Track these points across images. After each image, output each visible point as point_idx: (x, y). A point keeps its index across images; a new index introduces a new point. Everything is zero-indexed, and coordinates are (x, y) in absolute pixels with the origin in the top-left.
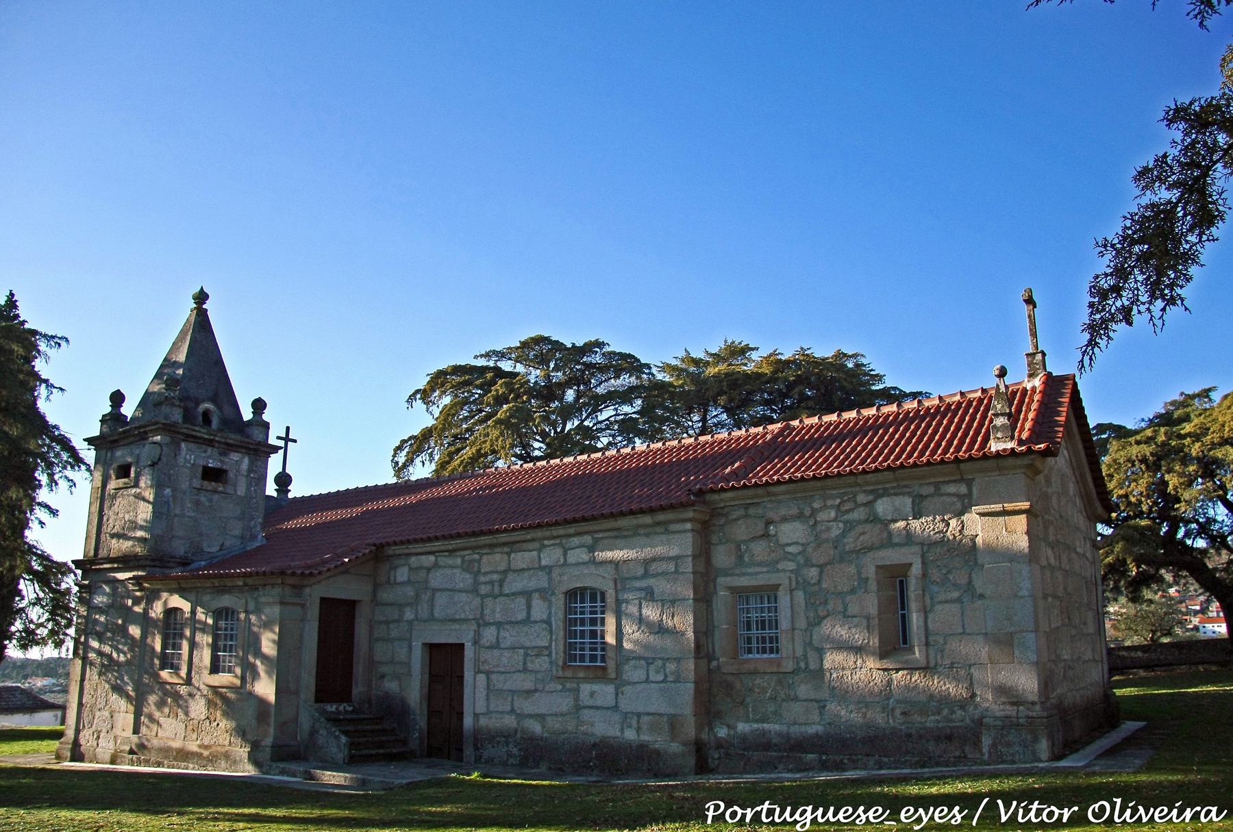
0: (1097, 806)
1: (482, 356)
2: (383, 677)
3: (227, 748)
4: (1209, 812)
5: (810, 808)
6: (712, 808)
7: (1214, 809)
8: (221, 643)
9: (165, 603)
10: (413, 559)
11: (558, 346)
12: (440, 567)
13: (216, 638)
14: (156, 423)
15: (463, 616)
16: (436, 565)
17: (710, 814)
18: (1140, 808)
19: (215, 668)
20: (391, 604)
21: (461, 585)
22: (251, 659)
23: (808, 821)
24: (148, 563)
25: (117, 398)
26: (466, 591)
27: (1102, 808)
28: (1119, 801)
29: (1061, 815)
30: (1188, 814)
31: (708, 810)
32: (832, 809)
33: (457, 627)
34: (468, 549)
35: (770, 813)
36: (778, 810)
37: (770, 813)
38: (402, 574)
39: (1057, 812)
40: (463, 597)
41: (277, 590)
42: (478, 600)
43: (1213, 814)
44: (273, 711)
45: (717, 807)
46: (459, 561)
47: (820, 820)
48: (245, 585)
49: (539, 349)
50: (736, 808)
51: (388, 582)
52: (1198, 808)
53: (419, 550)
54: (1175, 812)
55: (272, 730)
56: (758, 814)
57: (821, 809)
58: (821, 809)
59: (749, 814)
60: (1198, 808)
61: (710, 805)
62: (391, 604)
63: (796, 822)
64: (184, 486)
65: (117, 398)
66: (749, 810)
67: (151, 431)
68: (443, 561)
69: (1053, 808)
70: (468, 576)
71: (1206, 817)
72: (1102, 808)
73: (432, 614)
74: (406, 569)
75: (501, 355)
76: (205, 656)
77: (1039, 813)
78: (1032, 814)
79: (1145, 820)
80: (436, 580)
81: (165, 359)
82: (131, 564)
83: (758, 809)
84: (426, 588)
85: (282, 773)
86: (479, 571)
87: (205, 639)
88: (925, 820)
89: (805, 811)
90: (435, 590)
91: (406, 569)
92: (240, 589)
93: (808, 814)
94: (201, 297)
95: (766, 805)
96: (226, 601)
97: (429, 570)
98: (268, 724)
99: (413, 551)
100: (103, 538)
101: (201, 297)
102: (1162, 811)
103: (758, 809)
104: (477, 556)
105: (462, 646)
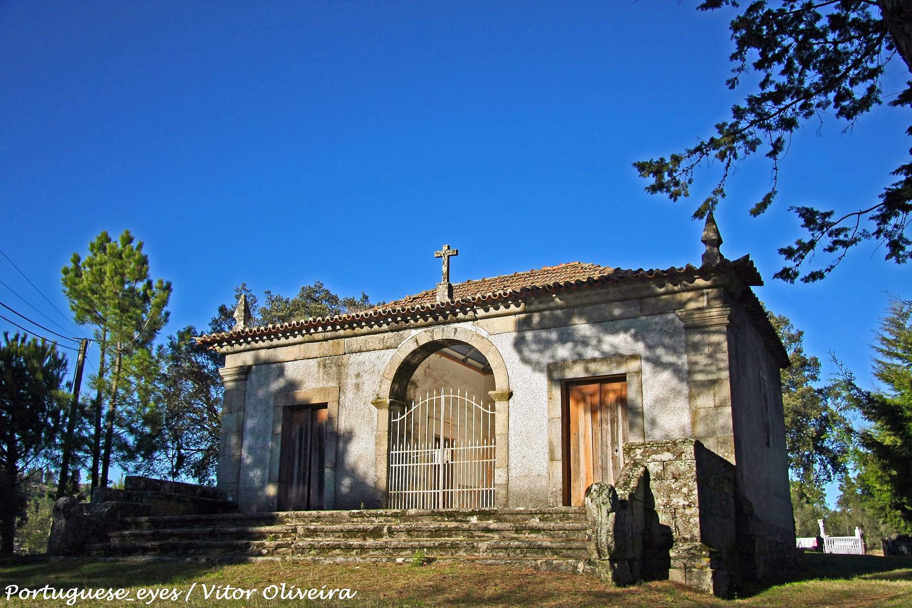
0: (269, 588)
6: (10, 590)
28: (284, 585)
29: (245, 595)
35: (49, 592)
39: (29, 592)
43: (348, 594)
45: (13, 589)
50: (26, 590)
56: (337, 593)
61: (9, 588)
69: (240, 590)
77: (230, 592)
78: (226, 594)
89: (72, 592)
95: (47, 588)
103: (41, 590)
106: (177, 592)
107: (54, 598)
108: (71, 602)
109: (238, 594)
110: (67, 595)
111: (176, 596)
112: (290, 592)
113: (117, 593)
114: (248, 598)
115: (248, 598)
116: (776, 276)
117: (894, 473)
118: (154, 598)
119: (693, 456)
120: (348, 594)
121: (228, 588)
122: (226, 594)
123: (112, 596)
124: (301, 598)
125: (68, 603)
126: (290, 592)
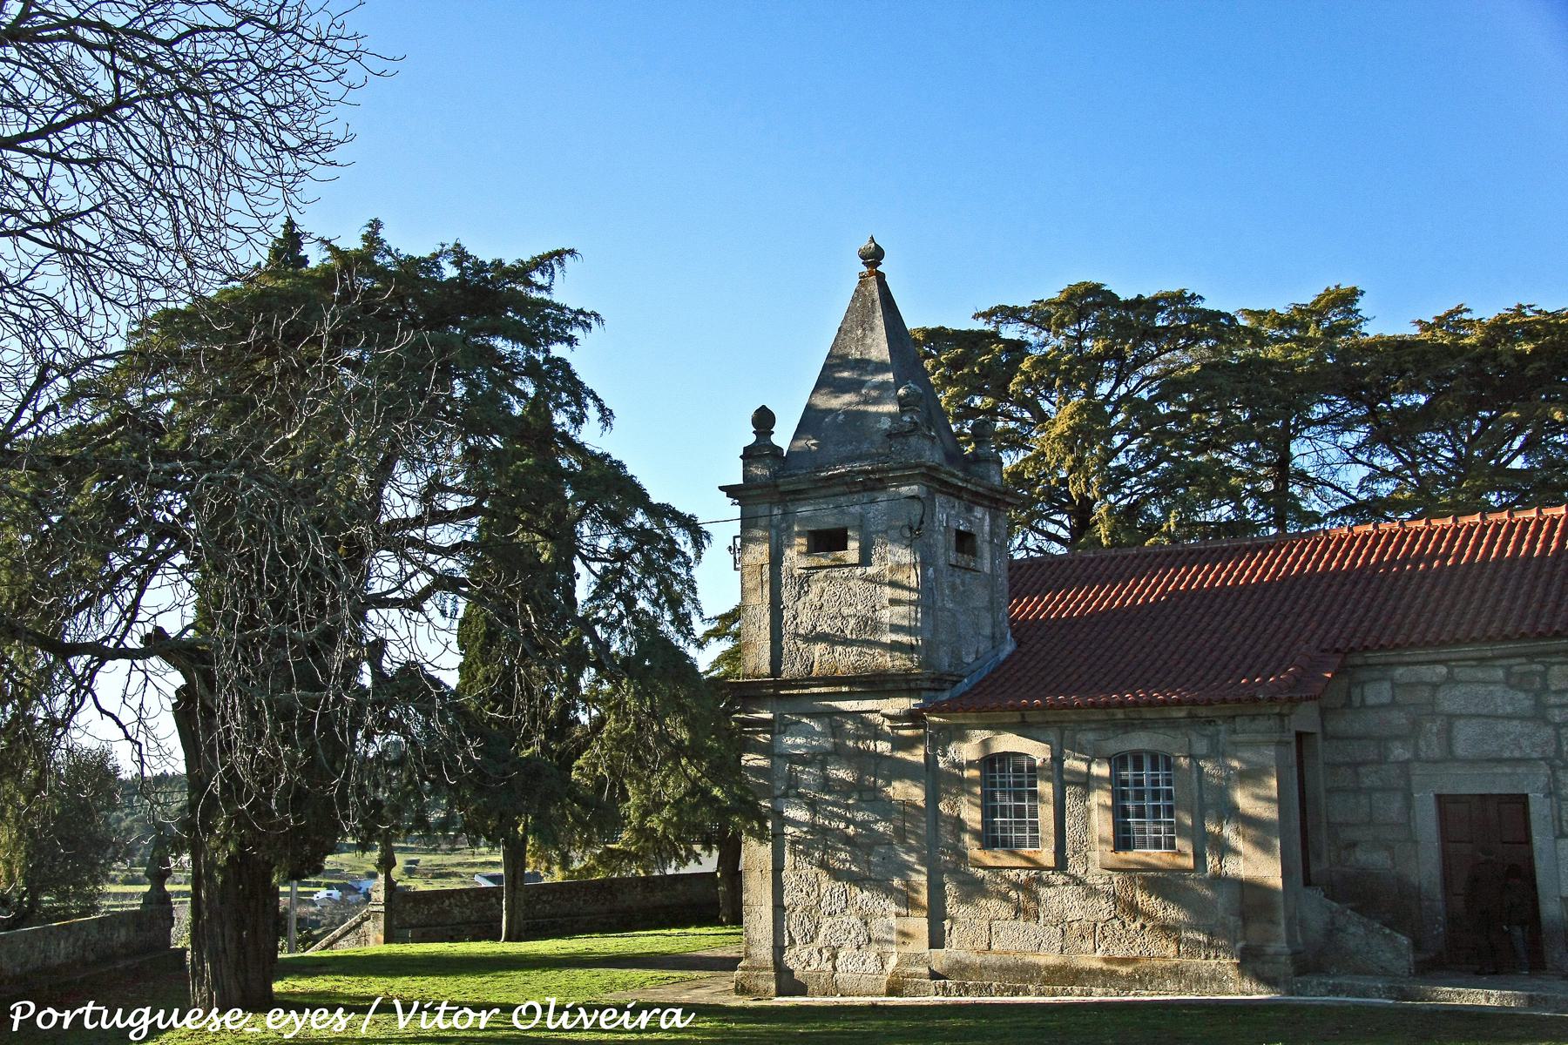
1: (984, 315)
2: (1353, 845)
3: (1176, 961)
5: (147, 1011)
6: (19, 1010)
8: (1131, 805)
9: (985, 744)
10: (1400, 671)
11: (1111, 298)
12: (1458, 682)
13: (1119, 796)
14: (917, 466)
15: (1517, 754)
16: (1450, 680)
17: (17, 1018)
19: (1123, 840)
20: (1360, 738)
21: (1509, 709)
22: (1212, 827)
23: (145, 1028)
24: (927, 685)
25: (764, 420)
26: (1522, 718)
29: (61, 1020)
31: (14, 1012)
32: (176, 1011)
33: (1507, 770)
34: (1521, 656)
35: (95, 1016)
36: (105, 1013)
37: (95, 1016)
38: (1379, 693)
39: (55, 1015)
40: (1516, 726)
41: (1262, 724)
42: (1550, 731)
43: (677, 1018)
44: (1280, 899)
45: (25, 1009)
46: (1500, 673)
47: (161, 1026)
48: (1191, 716)
49: (1087, 301)
50: (50, 1010)
51: (1348, 704)
53: (1421, 658)
55: (1282, 930)
56: (80, 1017)
57: (162, 1012)
58: (162, 1012)
59: (68, 1018)
61: (17, 1006)
62: (1360, 738)
63: (129, 1028)
64: (941, 562)
65: (764, 420)
66: (68, 1012)
67: (894, 479)
68: (1461, 673)
70: (1521, 695)
71: (667, 1022)
73: (1451, 752)
74: (1387, 685)
75: (1012, 314)
76: (1102, 825)
79: (587, 1025)
80: (1451, 700)
81: (829, 356)
82: (889, 686)
83: (80, 1011)
84: (1433, 713)
85: (1335, 990)
86: (1545, 688)
87: (1101, 798)
88: (299, 1025)
89: (140, 1015)
90: (1451, 717)
91: (1387, 685)
92: (1172, 724)
93: (145, 1018)
94: (873, 257)
95: (90, 1007)
96: (1139, 741)
97: (1435, 686)
98: (1272, 922)
99: (1407, 659)
100: (787, 644)
101: (873, 257)
102: (196, 1014)
103: (80, 1011)
104: (1539, 668)
105: (1523, 800)
107: (104, 1026)
108: (137, 1035)
110: (130, 1021)
113: (227, 1017)
114: (66, 1026)
115: (66, 1026)
116: (721, 488)
117: (545, 556)
119: (451, 979)
120: (677, 1018)
125: (132, 1036)
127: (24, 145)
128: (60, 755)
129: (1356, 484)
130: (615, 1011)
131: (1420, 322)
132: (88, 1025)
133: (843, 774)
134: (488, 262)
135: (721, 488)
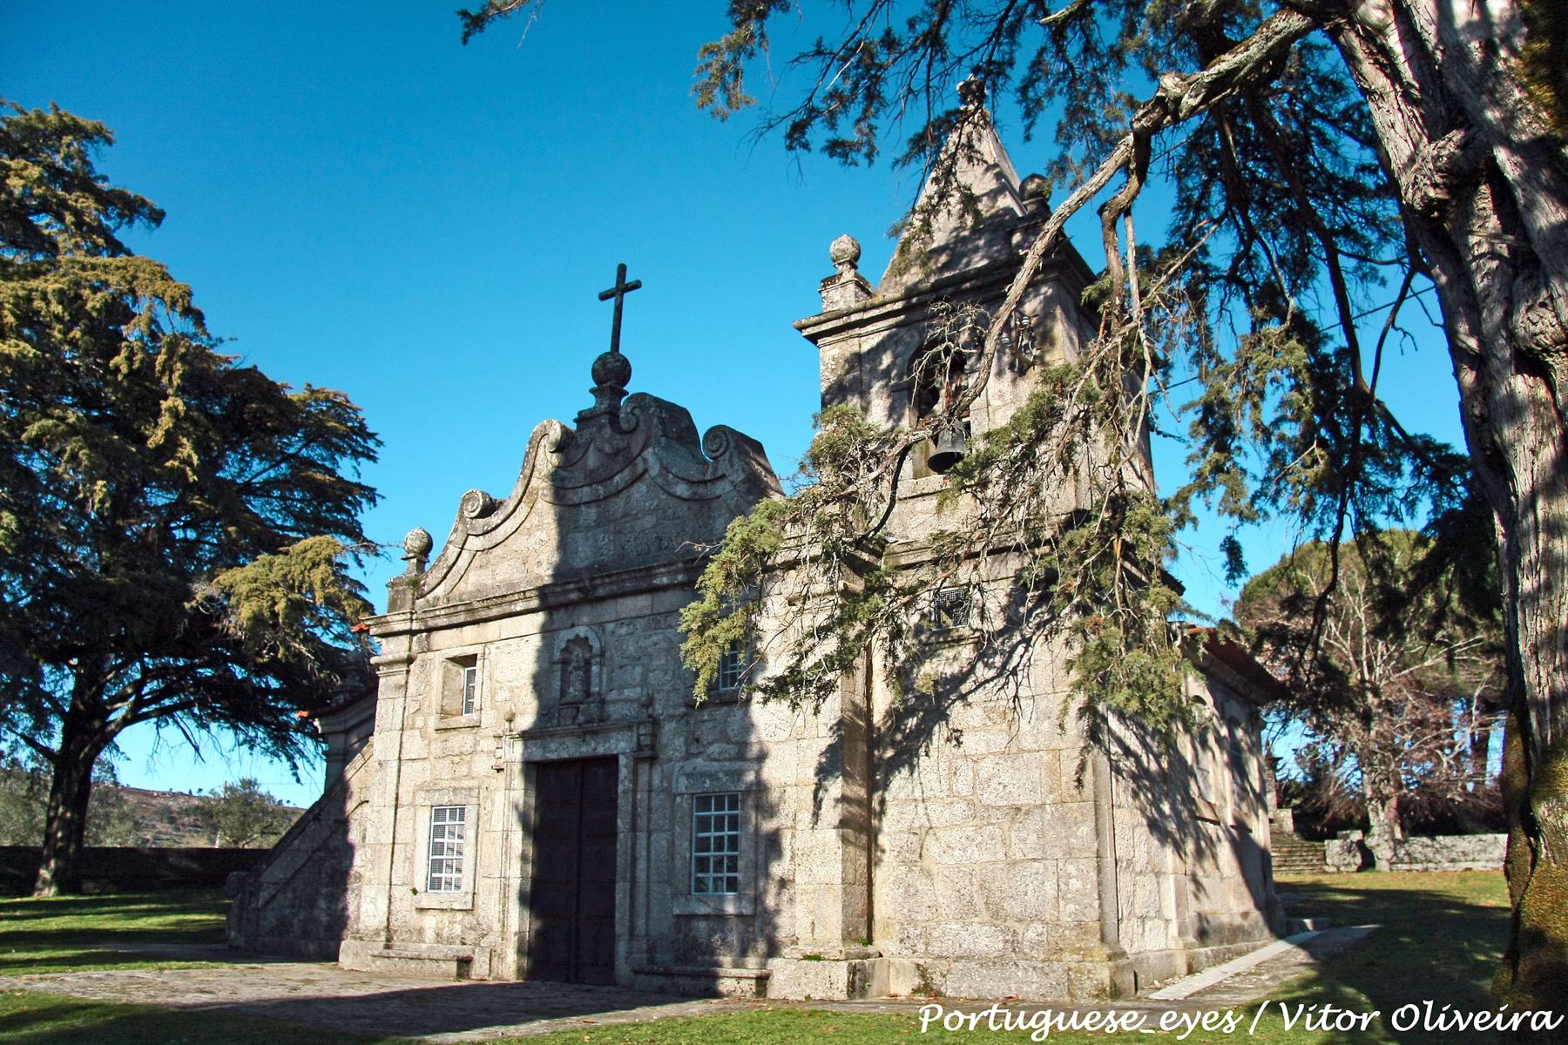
0: (1403, 1010)
4: (1541, 1018)
7: (1548, 1014)
17: (925, 1020)
18: (1457, 1012)
27: (1410, 1013)
28: (1430, 1004)
30: (1516, 1021)
35: (999, 1018)
36: (1009, 1015)
39: (962, 1017)
43: (1547, 1020)
45: (934, 1012)
52: (1528, 1013)
54: (1499, 1018)
57: (1062, 1015)
59: (974, 1020)
60: (1528, 1013)
63: (1032, 1030)
69: (1349, 1013)
72: (1410, 1013)
77: (1331, 1019)
78: (1323, 1020)
83: (985, 1013)
89: (1041, 1017)
103: (985, 1013)
106: (1234, 1018)
109: (1346, 1021)
110: (1032, 1023)
111: (1232, 1024)
112: (1442, 1017)
118: (1191, 1027)
120: (1547, 1020)
121: (1327, 1010)
122: (1323, 1020)
123: (1114, 1024)
124: (1462, 1027)
125: (1034, 1037)
126: (1442, 1017)
127: (943, 258)
128: (185, 440)
129: (1411, 850)
130: (1099, 1015)
131: (897, 162)
132: (992, 1027)
133: (912, 722)
134: (589, 402)
135: (465, 42)
